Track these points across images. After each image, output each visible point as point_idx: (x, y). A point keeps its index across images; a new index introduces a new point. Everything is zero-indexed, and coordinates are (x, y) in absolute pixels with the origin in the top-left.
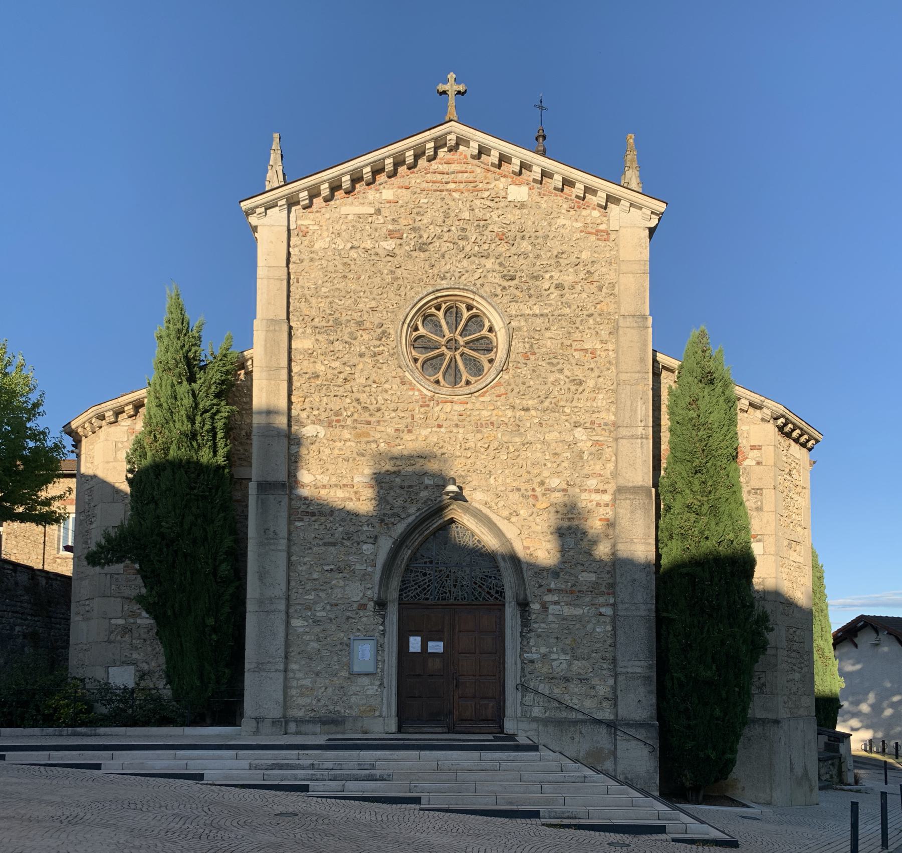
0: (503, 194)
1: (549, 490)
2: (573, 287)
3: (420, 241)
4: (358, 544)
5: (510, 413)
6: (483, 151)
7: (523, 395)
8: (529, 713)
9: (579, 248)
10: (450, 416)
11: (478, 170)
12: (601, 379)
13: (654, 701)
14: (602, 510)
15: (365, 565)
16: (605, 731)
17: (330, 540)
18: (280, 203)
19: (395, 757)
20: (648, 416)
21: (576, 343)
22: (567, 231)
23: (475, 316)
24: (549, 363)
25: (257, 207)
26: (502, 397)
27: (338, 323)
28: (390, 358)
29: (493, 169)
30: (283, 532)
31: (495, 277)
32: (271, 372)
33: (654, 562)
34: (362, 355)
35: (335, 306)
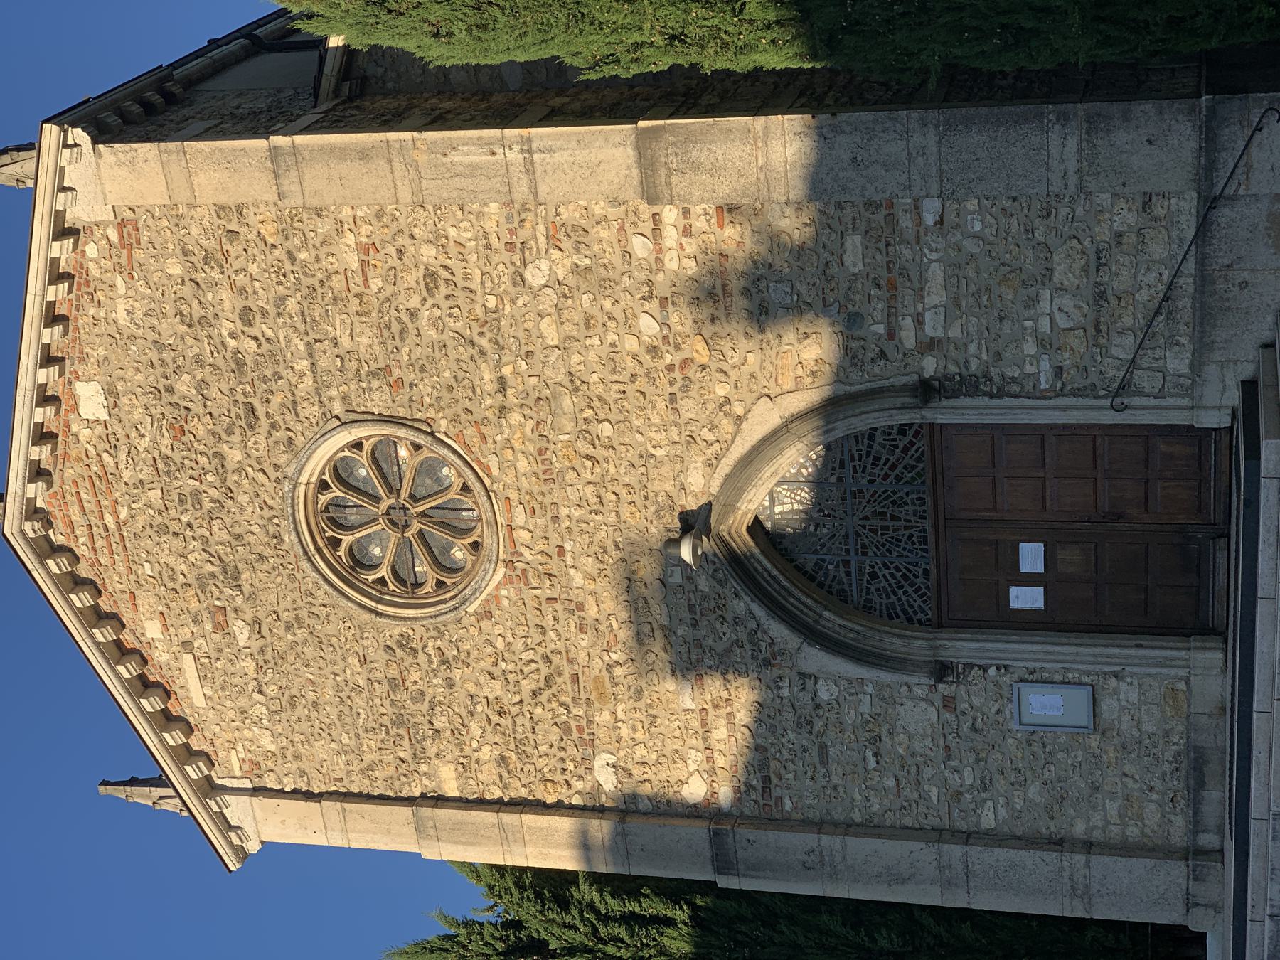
0: (99, 430)
1: (665, 337)
2: (242, 291)
3: (221, 578)
4: (818, 706)
5: (515, 417)
6: (38, 473)
7: (474, 392)
8: (1181, 380)
9: (164, 280)
10: (539, 532)
11: (69, 473)
12: (416, 231)
13: (1148, 106)
14: (699, 224)
15: (861, 696)
16: (1226, 211)
17: (815, 752)
18: (216, 809)
19: (1264, 756)
20: (480, 138)
21: (352, 285)
22: (137, 305)
23: (336, 472)
24: (402, 340)
25: (231, 844)
26: (485, 432)
27: (400, 721)
28: (447, 637)
29: (60, 446)
30: (808, 840)
31: (256, 443)
32: (510, 837)
33: (808, 117)
34: (450, 683)
35: (370, 725)
